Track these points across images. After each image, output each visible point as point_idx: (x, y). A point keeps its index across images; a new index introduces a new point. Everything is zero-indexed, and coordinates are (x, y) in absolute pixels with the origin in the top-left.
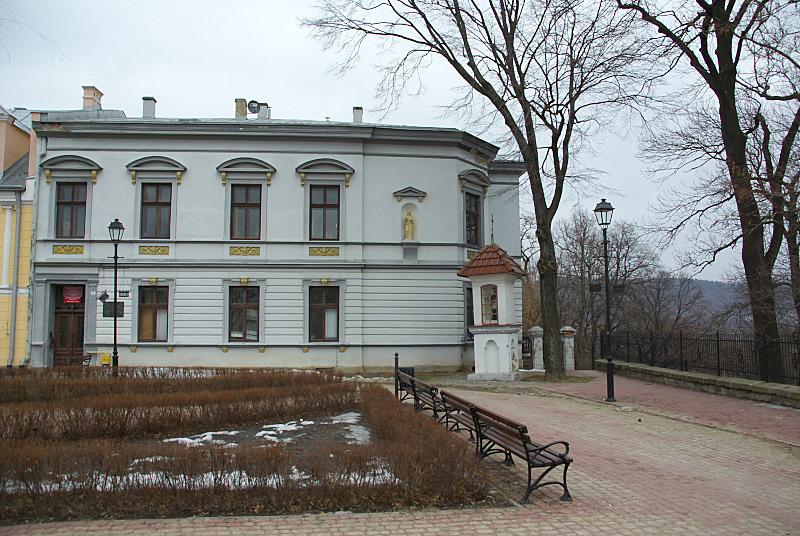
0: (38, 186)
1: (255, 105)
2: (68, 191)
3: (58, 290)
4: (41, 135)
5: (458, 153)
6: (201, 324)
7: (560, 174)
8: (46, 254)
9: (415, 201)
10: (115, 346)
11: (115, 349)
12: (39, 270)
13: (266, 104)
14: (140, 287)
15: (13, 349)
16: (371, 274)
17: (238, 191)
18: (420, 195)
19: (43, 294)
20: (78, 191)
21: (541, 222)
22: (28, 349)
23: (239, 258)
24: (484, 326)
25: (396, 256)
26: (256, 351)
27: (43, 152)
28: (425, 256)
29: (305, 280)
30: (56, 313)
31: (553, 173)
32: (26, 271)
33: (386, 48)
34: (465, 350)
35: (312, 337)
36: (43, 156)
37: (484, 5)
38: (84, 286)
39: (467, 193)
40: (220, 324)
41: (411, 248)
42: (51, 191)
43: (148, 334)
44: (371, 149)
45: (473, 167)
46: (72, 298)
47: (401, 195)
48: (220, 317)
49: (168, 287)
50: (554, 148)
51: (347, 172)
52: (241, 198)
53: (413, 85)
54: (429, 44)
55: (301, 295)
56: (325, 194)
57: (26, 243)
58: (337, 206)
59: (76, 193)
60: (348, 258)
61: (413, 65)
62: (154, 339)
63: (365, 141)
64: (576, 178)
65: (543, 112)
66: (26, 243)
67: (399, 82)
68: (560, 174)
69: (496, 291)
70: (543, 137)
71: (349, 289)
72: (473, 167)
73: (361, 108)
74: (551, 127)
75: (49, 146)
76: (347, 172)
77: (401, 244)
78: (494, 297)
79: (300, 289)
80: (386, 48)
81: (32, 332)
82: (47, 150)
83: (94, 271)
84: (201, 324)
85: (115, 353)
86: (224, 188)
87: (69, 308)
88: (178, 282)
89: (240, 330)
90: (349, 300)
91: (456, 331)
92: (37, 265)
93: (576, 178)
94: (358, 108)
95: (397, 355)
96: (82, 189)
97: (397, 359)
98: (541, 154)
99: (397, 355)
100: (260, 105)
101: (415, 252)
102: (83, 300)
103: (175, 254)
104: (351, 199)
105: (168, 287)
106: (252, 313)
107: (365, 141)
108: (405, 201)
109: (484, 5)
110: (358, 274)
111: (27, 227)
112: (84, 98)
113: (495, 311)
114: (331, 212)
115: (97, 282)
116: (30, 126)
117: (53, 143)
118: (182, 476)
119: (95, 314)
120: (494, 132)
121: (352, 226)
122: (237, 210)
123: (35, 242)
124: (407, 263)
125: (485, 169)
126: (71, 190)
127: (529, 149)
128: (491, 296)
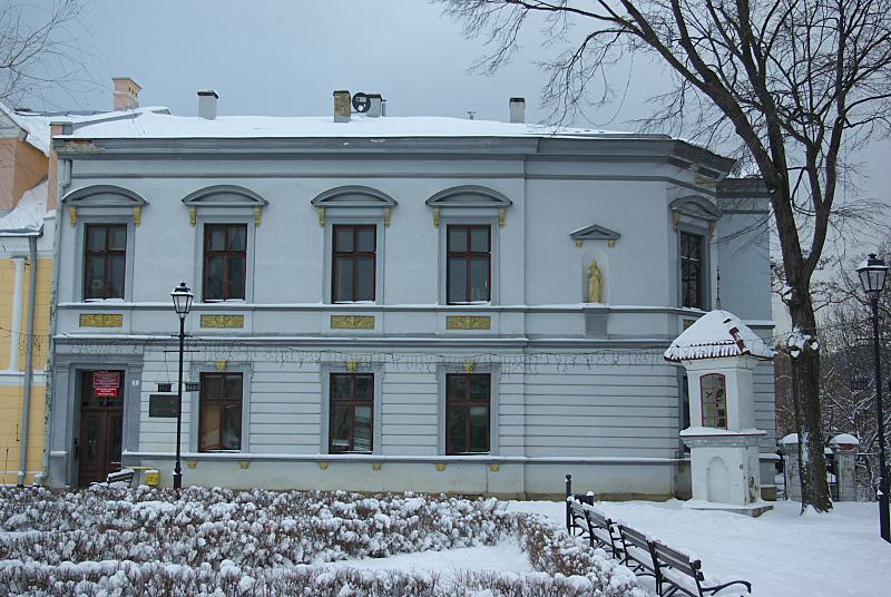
1: (364, 100)
3: (86, 378)
4: (69, 159)
5: (669, 171)
6: (289, 429)
7: (823, 208)
8: (70, 328)
11: (178, 464)
12: (62, 349)
13: (379, 96)
14: (447, 375)
16: (135, 312)
17: (341, 235)
18: (610, 236)
19: (66, 384)
21: (793, 278)
22: (45, 463)
25: (575, 328)
26: (369, 467)
27: (66, 181)
28: (616, 327)
29: (324, 365)
30: (82, 410)
31: (810, 205)
32: (45, 352)
33: (555, 34)
34: (681, 471)
35: (451, 448)
36: (66, 187)
37: (698, 17)
38: (122, 372)
39: (682, 233)
40: (317, 429)
41: (596, 318)
42: (77, 237)
44: (535, 168)
45: (689, 192)
46: (105, 389)
47: (582, 236)
48: (317, 419)
49: (242, 374)
50: (811, 168)
52: (346, 244)
53: (595, 88)
54: (617, 19)
55: (319, 386)
56: (469, 237)
57: (44, 311)
58: (487, 256)
60: (504, 331)
61: (593, 59)
63: (527, 158)
64: (845, 213)
65: (788, 122)
66: (44, 311)
67: (577, 84)
68: (823, 208)
69: (723, 384)
70: (795, 153)
71: (505, 379)
72: (689, 192)
73: (522, 100)
74: (805, 140)
75: (75, 171)
77: (583, 310)
78: (721, 392)
79: (316, 378)
80: (555, 34)
81: (51, 437)
82: (71, 177)
83: (139, 350)
84: (289, 429)
85: (178, 470)
86: (322, 230)
87: (101, 404)
88: (257, 367)
89: (343, 438)
91: (665, 402)
92: (56, 342)
93: (845, 213)
94: (517, 100)
95: (569, 477)
96: (120, 233)
97: (569, 484)
98: (793, 177)
99: (569, 477)
100: (369, 97)
101: (604, 324)
102: (120, 391)
103: (253, 325)
104: (507, 248)
105: (242, 374)
106: (361, 413)
107: (527, 158)
109: (698, 17)
110: (516, 357)
111: (45, 289)
112: (116, 95)
113: (723, 413)
114: (477, 264)
115: (142, 366)
116: (48, 142)
117: (81, 167)
118: (788, 288)
120: (727, 142)
122: (341, 262)
123: (55, 310)
125: (712, 194)
126: (104, 233)
127: (775, 170)
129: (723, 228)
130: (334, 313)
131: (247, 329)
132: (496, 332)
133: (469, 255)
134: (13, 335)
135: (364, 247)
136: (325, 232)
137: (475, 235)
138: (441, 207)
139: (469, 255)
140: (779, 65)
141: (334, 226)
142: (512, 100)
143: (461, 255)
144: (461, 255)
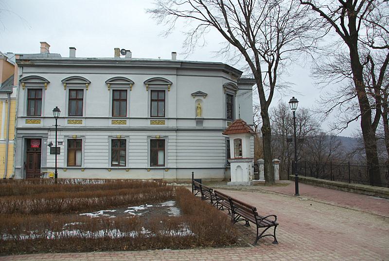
0: (19, 90)
2: (33, 93)
3: (28, 141)
4: (20, 66)
5: (223, 75)
6: (98, 158)
7: (272, 85)
8: (22, 124)
9: (202, 98)
10: (56, 168)
11: (56, 170)
12: (19, 132)
14: (68, 140)
15: (6, 170)
17: (116, 93)
18: (204, 95)
19: (21, 143)
20: (38, 93)
21: (263, 108)
22: (14, 170)
23: (116, 126)
24: (235, 159)
25: (192, 124)
26: (125, 171)
27: (21, 74)
28: (207, 125)
29: (148, 137)
30: (27, 152)
31: (269, 84)
32: (13, 132)
34: (226, 170)
35: (152, 164)
36: (21, 76)
38: (41, 139)
39: (227, 94)
40: (107, 158)
41: (200, 121)
42: (25, 93)
43: (72, 163)
44: (180, 73)
45: (230, 82)
46: (35, 145)
47: (195, 95)
48: (107, 154)
49: (81, 140)
50: (269, 72)
51: (169, 84)
52: (117, 97)
54: (208, 21)
55: (147, 144)
56: (158, 94)
57: (13, 118)
58: (164, 100)
59: (37, 94)
60: (169, 126)
62: (75, 165)
63: (177, 69)
64: (280, 87)
65: (264, 55)
66: (13, 118)
68: (272, 85)
69: (241, 142)
70: (264, 67)
71: (170, 141)
72: (230, 82)
74: (268, 62)
75: (24, 71)
76: (169, 84)
77: (195, 119)
78: (240, 145)
79: (146, 141)
81: (15, 162)
82: (23, 73)
83: (46, 132)
84: (98, 158)
85: (56, 172)
86: (109, 92)
87: (34, 150)
88: (87, 137)
89: (117, 161)
90: (170, 146)
92: (18, 129)
93: (280, 87)
95: (193, 173)
96: (40, 92)
97: (193, 175)
98: (263, 75)
99: (193, 173)
101: (202, 123)
102: (40, 146)
103: (85, 123)
104: (171, 97)
105: (81, 140)
106: (122, 153)
107: (177, 69)
108: (197, 98)
110: (174, 134)
111: (13, 110)
113: (241, 151)
114: (161, 103)
115: (47, 137)
116: (15, 61)
117: (26, 70)
119: (46, 153)
120: (240, 64)
121: (171, 110)
122: (115, 102)
123: (17, 118)
124: (198, 128)
126: (34, 92)
127: (257, 73)
128: (239, 144)
129: (239, 92)
130: (69, 119)
131: (166, 125)
132: (84, 125)
133: (35, 99)
134: (119, 125)
135: (80, 97)
136: (148, 93)
137: (123, 93)
138: (25, 83)
139: (119, 100)
140: (266, 37)
141: (69, 89)
142: (70, 48)
143: (117, 100)
144: (117, 100)
